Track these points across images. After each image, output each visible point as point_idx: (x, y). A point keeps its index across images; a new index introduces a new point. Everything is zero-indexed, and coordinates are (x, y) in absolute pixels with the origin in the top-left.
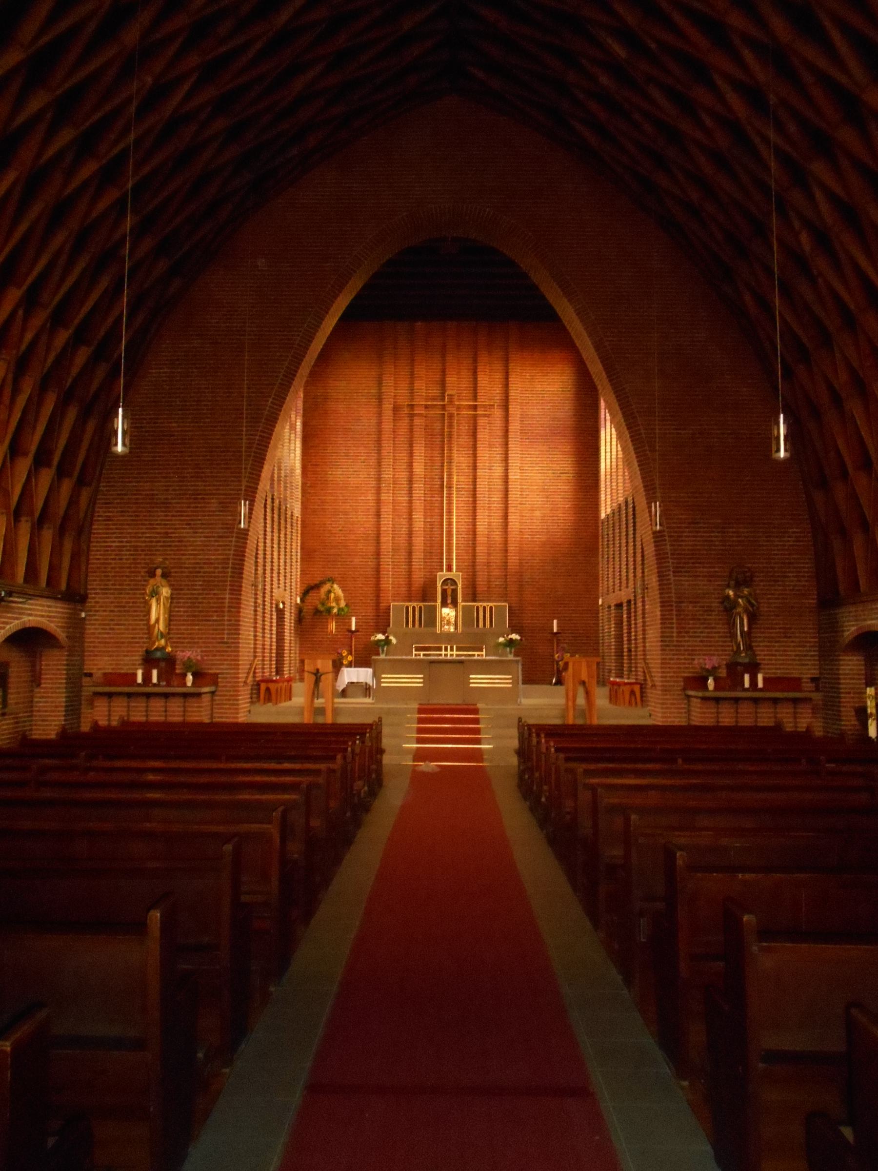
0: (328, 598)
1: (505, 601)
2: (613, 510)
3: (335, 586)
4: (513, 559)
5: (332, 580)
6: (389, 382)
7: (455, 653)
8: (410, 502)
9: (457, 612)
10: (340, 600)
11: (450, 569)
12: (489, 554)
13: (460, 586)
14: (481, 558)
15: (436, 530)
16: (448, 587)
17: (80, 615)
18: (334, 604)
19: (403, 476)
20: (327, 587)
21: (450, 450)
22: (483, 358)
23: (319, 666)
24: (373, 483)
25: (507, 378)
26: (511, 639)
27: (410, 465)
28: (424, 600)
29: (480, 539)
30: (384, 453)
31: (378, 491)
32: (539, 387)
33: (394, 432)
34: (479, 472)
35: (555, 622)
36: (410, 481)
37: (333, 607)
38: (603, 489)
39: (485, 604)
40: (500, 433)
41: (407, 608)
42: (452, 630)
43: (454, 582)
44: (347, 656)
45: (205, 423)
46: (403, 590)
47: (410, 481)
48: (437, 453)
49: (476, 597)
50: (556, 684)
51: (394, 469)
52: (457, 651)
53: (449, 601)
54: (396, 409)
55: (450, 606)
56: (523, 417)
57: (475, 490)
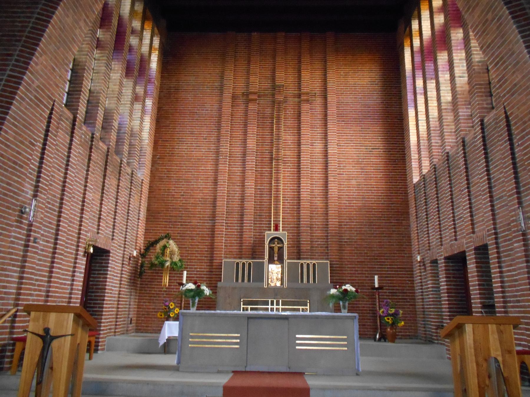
0: (163, 254)
1: (327, 259)
2: (435, 168)
4: (333, 221)
5: (168, 237)
6: (229, 75)
7: (280, 307)
8: (244, 172)
9: (282, 268)
11: (276, 229)
12: (311, 218)
13: (286, 244)
14: (305, 221)
15: (266, 198)
16: (276, 246)
18: (168, 259)
19: (238, 151)
21: (278, 129)
22: (306, 59)
23: (51, 326)
25: (325, 75)
26: (346, 290)
27: (245, 141)
28: (254, 258)
29: (305, 204)
30: (223, 131)
31: (217, 161)
32: (351, 81)
34: (303, 147)
35: (376, 277)
36: (244, 154)
37: (166, 261)
38: (414, 156)
39: (308, 262)
40: (320, 117)
41: (238, 264)
42: (278, 284)
43: (280, 240)
44: (174, 309)
46: (235, 249)
47: (244, 154)
48: (267, 132)
49: (300, 255)
50: (380, 340)
51: (230, 144)
52: (282, 305)
53: (276, 259)
54: (234, 97)
55: (276, 262)
56: (339, 104)
57: (299, 162)
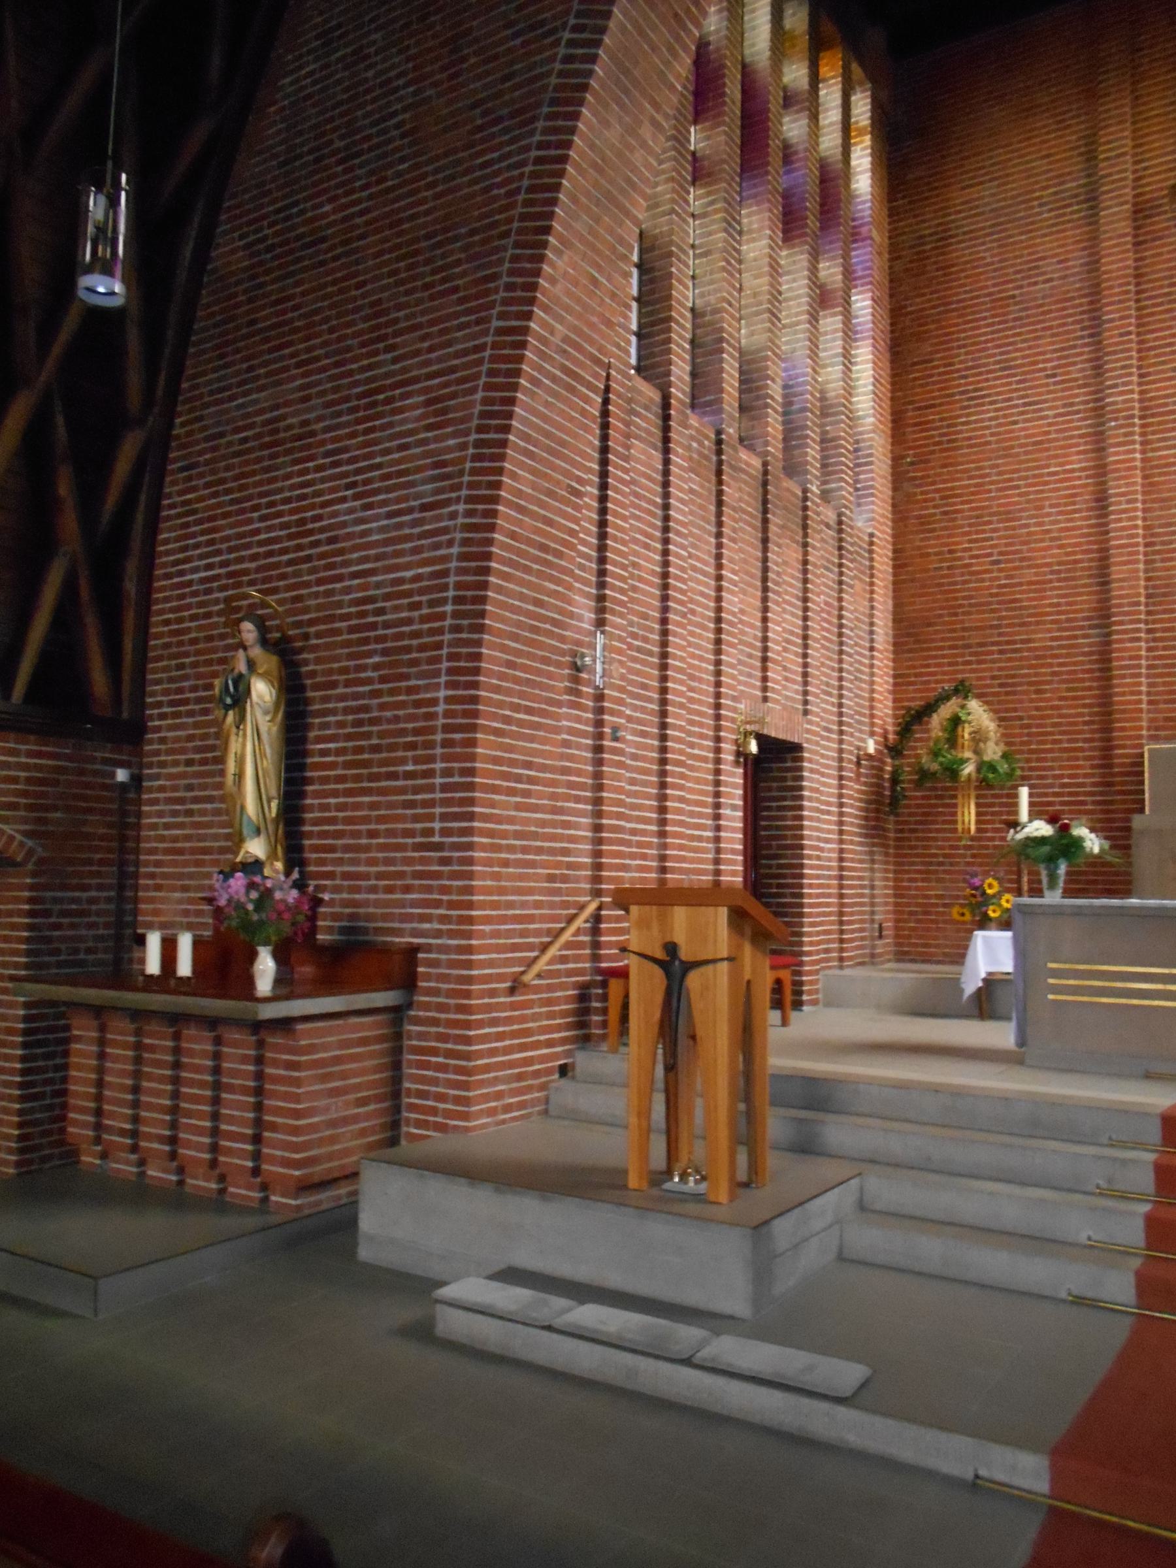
3: (974, 705)
5: (962, 690)
10: (986, 740)
17: (113, 775)
18: (968, 754)
20: (946, 711)
23: (680, 936)
24: (1082, 425)
30: (1111, 337)
31: (1099, 443)
33: (1136, 276)
37: (964, 761)
44: (998, 895)
45: (399, 174)
